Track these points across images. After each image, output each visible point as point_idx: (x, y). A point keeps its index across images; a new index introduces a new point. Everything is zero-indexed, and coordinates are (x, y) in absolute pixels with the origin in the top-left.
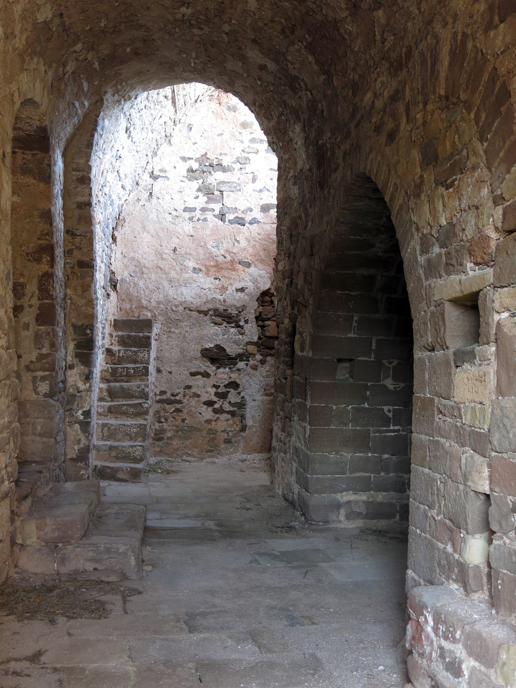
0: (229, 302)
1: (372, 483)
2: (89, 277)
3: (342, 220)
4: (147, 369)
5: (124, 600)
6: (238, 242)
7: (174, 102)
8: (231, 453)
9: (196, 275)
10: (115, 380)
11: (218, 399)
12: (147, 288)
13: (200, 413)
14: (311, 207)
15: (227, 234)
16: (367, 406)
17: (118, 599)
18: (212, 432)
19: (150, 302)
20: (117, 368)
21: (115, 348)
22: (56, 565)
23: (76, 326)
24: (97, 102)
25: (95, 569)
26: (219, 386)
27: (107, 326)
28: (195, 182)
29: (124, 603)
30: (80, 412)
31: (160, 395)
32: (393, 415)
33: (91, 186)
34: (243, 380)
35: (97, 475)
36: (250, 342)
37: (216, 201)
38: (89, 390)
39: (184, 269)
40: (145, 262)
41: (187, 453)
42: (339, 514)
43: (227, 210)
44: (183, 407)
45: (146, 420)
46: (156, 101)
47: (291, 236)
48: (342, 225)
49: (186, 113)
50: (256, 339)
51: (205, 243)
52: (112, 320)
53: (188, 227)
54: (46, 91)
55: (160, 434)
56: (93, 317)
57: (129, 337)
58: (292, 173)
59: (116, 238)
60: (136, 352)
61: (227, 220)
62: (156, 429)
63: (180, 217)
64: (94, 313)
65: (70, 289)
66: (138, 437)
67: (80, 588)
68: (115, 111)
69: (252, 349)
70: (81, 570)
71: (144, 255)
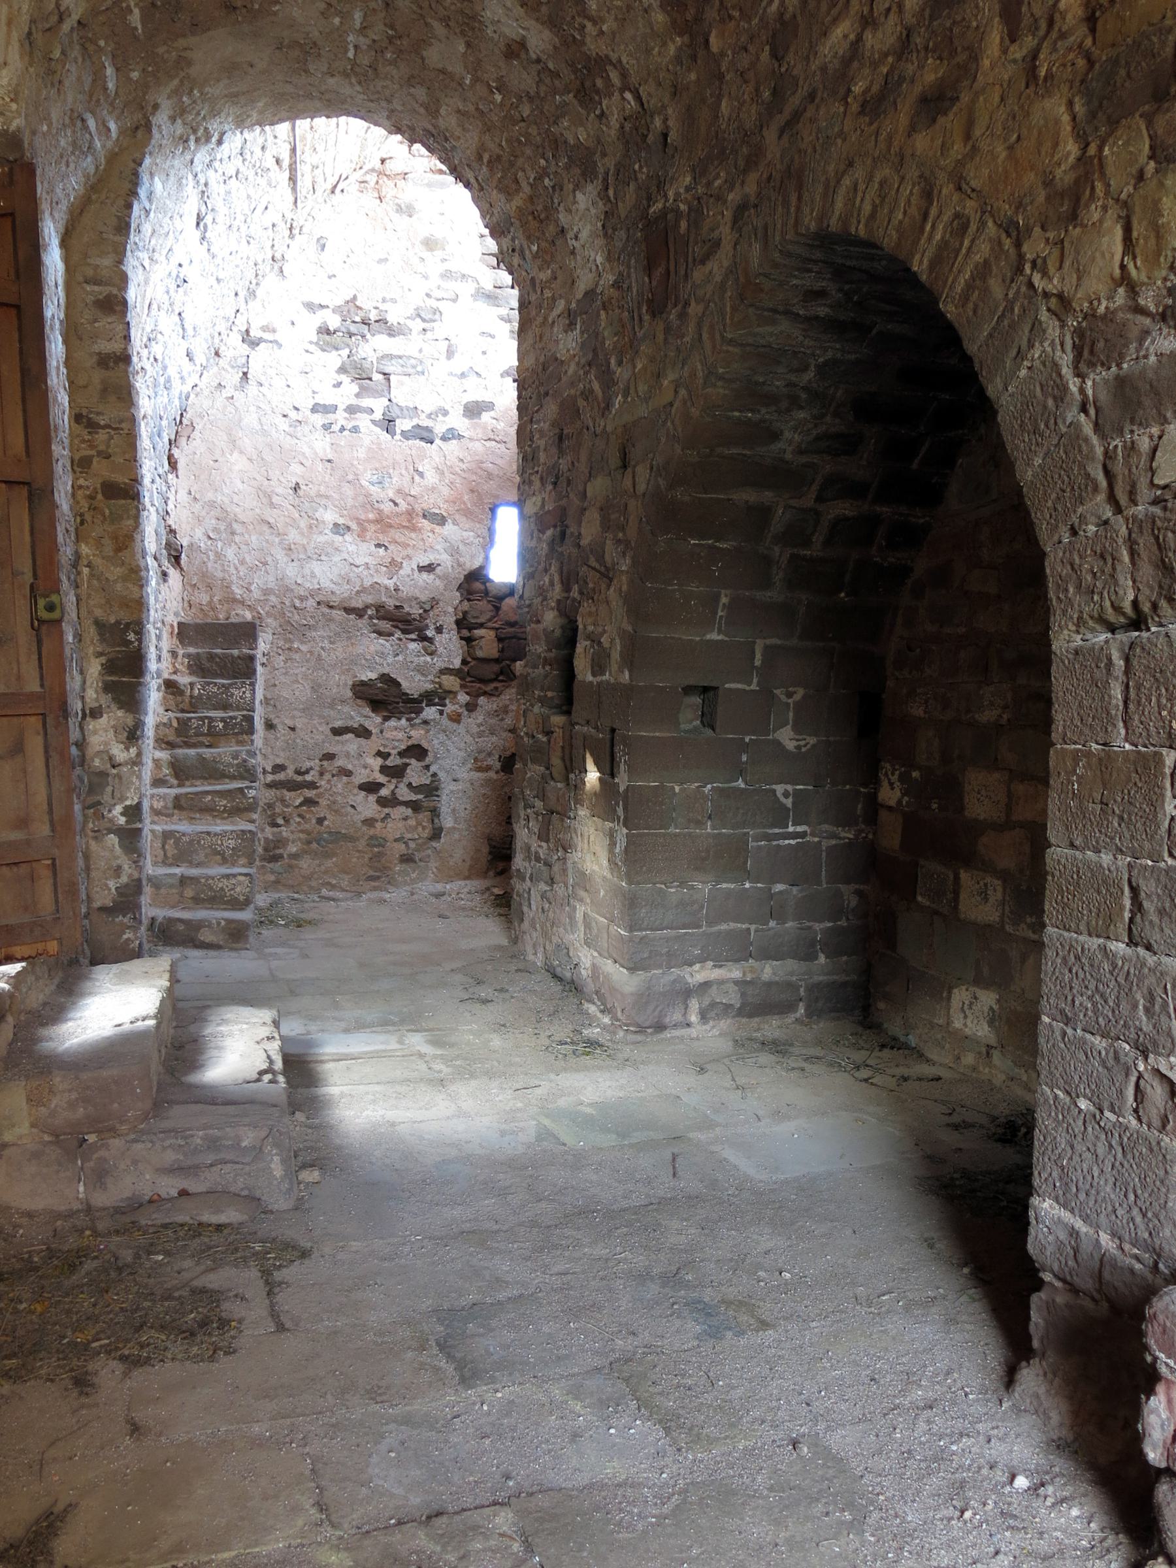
0: (406, 591)
1: (751, 944)
2: (128, 518)
3: (721, 370)
4: (250, 720)
5: (267, 1283)
6: (421, 475)
7: (293, 179)
8: (413, 881)
9: (341, 538)
10: (185, 743)
11: (387, 779)
12: (242, 562)
13: (353, 806)
14: (620, 363)
15: (398, 457)
16: (743, 786)
17: (248, 1279)
18: (377, 842)
19: (250, 591)
20: (190, 719)
21: (184, 680)
22: (81, 1189)
23: (104, 625)
24: (137, 128)
25: (183, 1193)
26: (389, 754)
27: (165, 636)
28: (334, 353)
29: (269, 1293)
30: (118, 809)
31: (273, 773)
32: (794, 803)
33: (128, 318)
34: (433, 741)
35: (157, 937)
36: (447, 669)
37: (377, 394)
38: (137, 762)
39: (315, 525)
40: (237, 510)
41: (329, 883)
42: (686, 1009)
43: (399, 413)
44: (319, 795)
45: (253, 821)
46: (258, 165)
47: (561, 438)
48: (720, 383)
49: (313, 213)
50: (457, 663)
51: (356, 475)
52: (175, 625)
53: (321, 444)
54: (15, 35)
55: (275, 848)
56: (139, 605)
57: (211, 657)
58: (561, 305)
59: (176, 462)
60: (227, 688)
61: (398, 431)
62: (266, 839)
63: (306, 422)
64: (142, 597)
65: (87, 544)
66: (239, 857)
67: (149, 1253)
68: (176, 162)
69: (450, 682)
70: (147, 1198)
71: (235, 497)
